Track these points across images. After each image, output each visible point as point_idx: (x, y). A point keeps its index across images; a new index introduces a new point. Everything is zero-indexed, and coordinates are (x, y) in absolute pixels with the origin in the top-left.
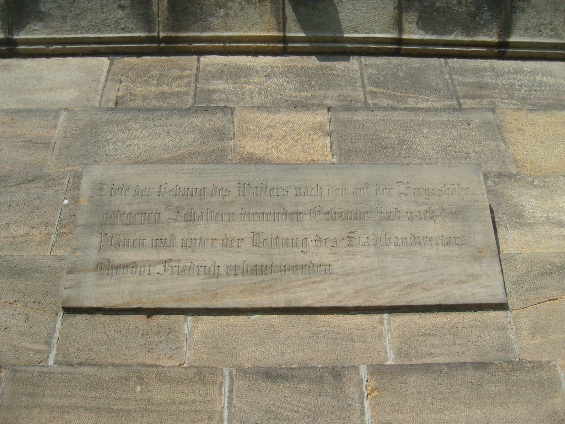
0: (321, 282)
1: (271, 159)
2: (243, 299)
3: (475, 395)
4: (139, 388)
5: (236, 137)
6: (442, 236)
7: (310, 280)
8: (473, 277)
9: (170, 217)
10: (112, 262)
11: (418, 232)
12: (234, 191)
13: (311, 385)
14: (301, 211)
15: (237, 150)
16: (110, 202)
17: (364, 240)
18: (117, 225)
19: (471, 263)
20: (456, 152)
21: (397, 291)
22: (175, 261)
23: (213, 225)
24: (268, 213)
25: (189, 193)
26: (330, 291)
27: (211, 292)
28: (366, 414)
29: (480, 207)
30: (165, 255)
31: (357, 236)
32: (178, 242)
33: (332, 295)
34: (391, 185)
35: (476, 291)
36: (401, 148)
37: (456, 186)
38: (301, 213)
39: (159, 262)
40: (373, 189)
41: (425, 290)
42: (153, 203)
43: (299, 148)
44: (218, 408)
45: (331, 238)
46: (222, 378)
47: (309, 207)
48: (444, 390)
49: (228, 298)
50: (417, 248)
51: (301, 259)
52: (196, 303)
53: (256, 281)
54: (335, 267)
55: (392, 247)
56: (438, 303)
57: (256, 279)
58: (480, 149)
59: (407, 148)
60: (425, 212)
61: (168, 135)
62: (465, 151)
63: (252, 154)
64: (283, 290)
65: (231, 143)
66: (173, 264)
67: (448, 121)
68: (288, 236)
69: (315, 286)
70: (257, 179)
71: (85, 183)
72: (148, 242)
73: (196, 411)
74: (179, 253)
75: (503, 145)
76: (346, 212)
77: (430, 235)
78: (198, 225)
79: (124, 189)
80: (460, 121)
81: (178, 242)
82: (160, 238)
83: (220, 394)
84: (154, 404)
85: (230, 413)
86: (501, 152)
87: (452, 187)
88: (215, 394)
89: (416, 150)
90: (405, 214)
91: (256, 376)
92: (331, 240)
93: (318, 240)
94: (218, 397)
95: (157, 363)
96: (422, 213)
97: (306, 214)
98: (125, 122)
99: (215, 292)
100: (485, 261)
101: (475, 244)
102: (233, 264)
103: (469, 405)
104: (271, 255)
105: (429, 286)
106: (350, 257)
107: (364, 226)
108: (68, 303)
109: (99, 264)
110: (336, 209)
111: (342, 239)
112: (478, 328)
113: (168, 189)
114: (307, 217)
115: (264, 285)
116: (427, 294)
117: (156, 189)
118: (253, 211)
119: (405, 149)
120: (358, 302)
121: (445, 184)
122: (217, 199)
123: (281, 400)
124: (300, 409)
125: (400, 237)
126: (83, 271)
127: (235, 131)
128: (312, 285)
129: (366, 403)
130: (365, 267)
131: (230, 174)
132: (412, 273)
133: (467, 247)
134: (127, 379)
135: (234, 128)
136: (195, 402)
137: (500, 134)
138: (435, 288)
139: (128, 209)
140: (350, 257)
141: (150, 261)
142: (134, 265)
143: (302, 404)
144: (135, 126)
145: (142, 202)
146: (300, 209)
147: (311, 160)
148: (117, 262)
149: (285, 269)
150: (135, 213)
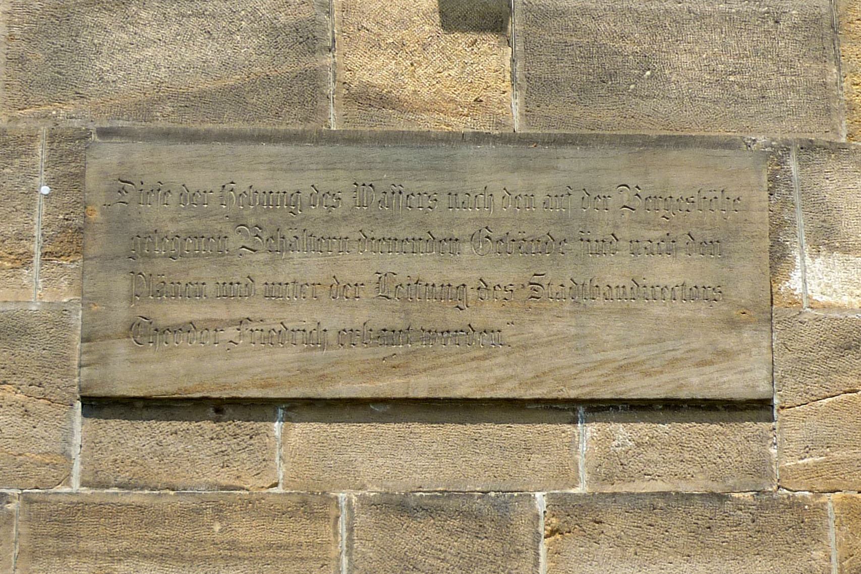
0: (484, 358)
1: (402, 97)
2: (364, 385)
3: (699, 543)
4: (217, 527)
5: (338, 46)
6: (683, 285)
7: (468, 355)
8: (725, 354)
9: (242, 244)
10: (154, 323)
11: (645, 277)
12: (347, 198)
13: (465, 523)
14: (456, 237)
15: (340, 76)
16: (139, 217)
17: (555, 288)
18: (155, 257)
19: (724, 331)
20: (742, 87)
21: (602, 375)
22: (256, 321)
23: (314, 259)
24: (402, 239)
25: (270, 200)
26: (499, 372)
27: (314, 372)
28: (541, 565)
29: (754, 234)
30: (240, 311)
31: (545, 283)
32: (259, 287)
33: (500, 381)
34: (607, 190)
35: (725, 379)
36: (640, 77)
37: (718, 194)
38: (457, 240)
39: (231, 323)
40: (576, 197)
41: (647, 374)
42: (213, 218)
43: (452, 73)
44: (333, 554)
45: (502, 284)
46: (337, 510)
47: (470, 230)
48: (656, 534)
49: (340, 384)
50: (641, 304)
51: (454, 319)
52: (291, 390)
53: (384, 356)
54: (508, 334)
55: (600, 302)
56: (663, 396)
57: (384, 351)
58: (788, 79)
59: (652, 76)
60: (659, 241)
61: (209, 38)
62: (759, 85)
63: (370, 85)
64: (425, 370)
65: (328, 59)
66: (253, 326)
67: (738, 12)
68: (434, 281)
69: (474, 364)
70: (385, 176)
71: (91, 179)
72: (210, 288)
73: (302, 559)
74: (261, 309)
75: (835, 70)
76: (531, 239)
77: (662, 283)
78: (290, 258)
79: (161, 190)
80: (761, 13)
81: (259, 287)
82: (229, 282)
83: (336, 534)
84: (242, 548)
85: (350, 560)
86: (828, 87)
87: (710, 195)
88: (329, 533)
89: (668, 81)
90: (626, 244)
91: (386, 507)
92: (503, 288)
93: (483, 286)
94: (332, 538)
95: (238, 483)
96: (655, 243)
97: (464, 241)
98: (123, 6)
99: (321, 373)
100: (747, 328)
101: (734, 299)
102: (348, 327)
103: (689, 556)
104: (407, 312)
105: (653, 367)
106: (532, 317)
107: (558, 265)
108: (90, 390)
109: (133, 325)
110: (514, 234)
111: (521, 286)
112: (721, 437)
113: (235, 193)
114: (466, 247)
115: (396, 362)
116: (647, 381)
117: (217, 193)
118: (378, 235)
119: (648, 79)
120: (539, 392)
121: (699, 189)
122: (316, 212)
123: (421, 544)
124: (449, 557)
125: (613, 285)
126: (108, 337)
127: (336, 31)
128: (469, 364)
129: (543, 549)
130: (554, 335)
131: (339, 166)
132: (628, 347)
133: (723, 305)
134: (199, 512)
135: (333, 26)
136: (300, 545)
137: (833, 46)
138: (661, 372)
139: (172, 228)
140: (532, 317)
141: (215, 320)
142: (189, 327)
143: (451, 549)
144: (143, 14)
145: (194, 217)
146: (456, 234)
147: (475, 101)
148: (161, 323)
149: (430, 335)
150: (183, 236)
